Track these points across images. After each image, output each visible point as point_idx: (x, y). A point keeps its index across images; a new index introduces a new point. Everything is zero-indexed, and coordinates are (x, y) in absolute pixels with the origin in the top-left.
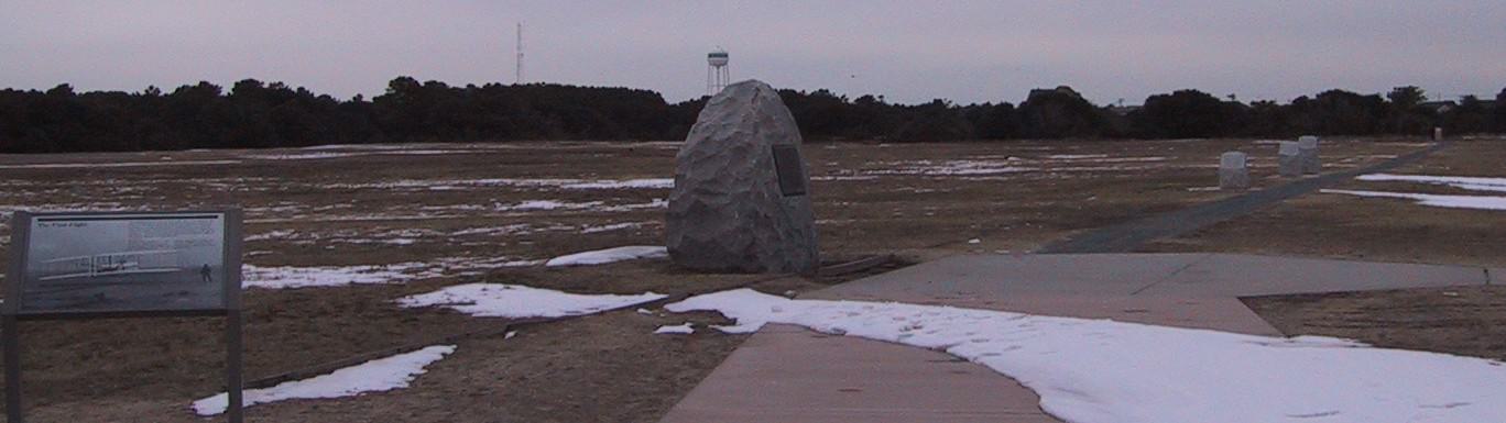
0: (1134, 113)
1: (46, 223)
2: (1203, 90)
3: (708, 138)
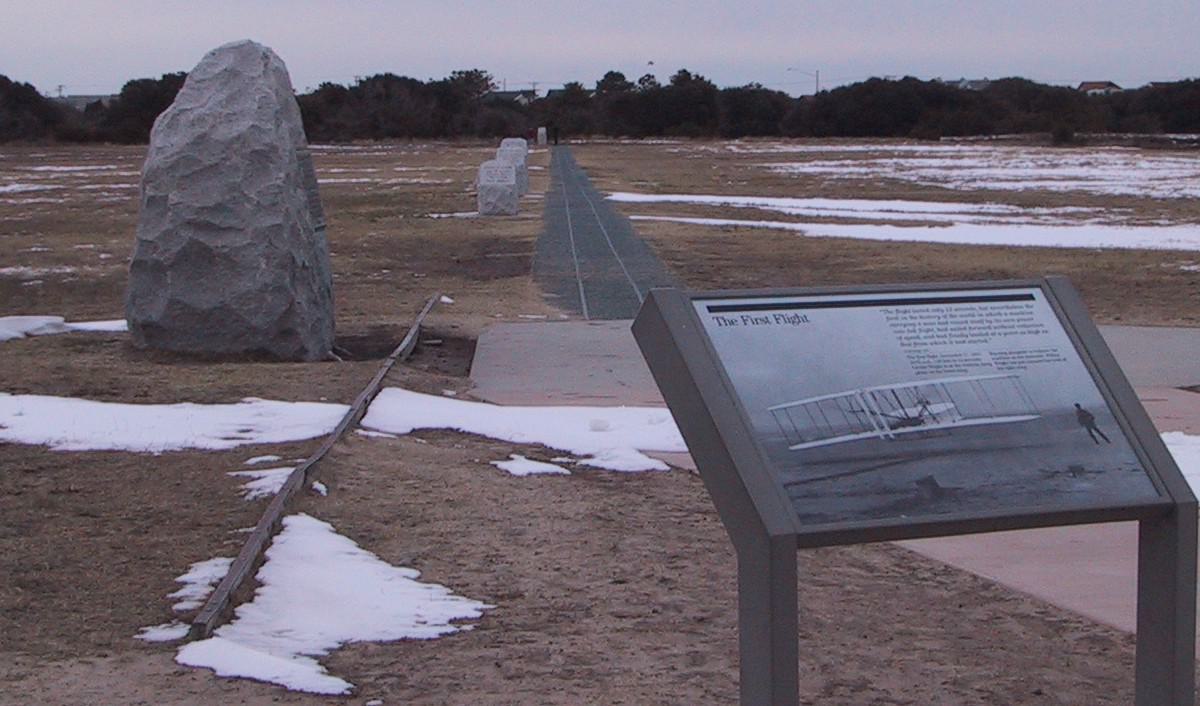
0: (95, 105)
1: (728, 315)
2: (1026, 77)
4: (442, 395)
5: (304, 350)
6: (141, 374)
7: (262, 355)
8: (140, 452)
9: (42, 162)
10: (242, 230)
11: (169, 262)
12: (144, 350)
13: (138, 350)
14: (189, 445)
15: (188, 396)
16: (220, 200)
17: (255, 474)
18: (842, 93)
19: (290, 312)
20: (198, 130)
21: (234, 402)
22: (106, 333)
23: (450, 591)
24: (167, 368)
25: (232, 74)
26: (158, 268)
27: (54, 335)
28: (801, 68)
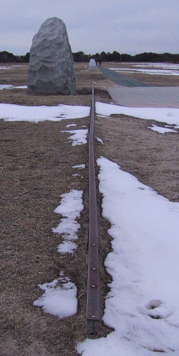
3: (45, 39)
4: (110, 104)
5: (70, 93)
6: (31, 98)
7: (60, 94)
8: (31, 122)
9: (14, 65)
10: (55, 63)
11: (37, 71)
12: (31, 92)
13: (30, 92)
14: (46, 119)
15: (43, 104)
16: (49, 55)
17: (71, 132)
18: (140, 55)
19: (67, 83)
20: (44, 38)
21: (57, 106)
22: (22, 89)
23: (120, 167)
24: (37, 96)
25: (52, 24)
26: (34, 72)
27: (10, 89)
28: (133, 51)
